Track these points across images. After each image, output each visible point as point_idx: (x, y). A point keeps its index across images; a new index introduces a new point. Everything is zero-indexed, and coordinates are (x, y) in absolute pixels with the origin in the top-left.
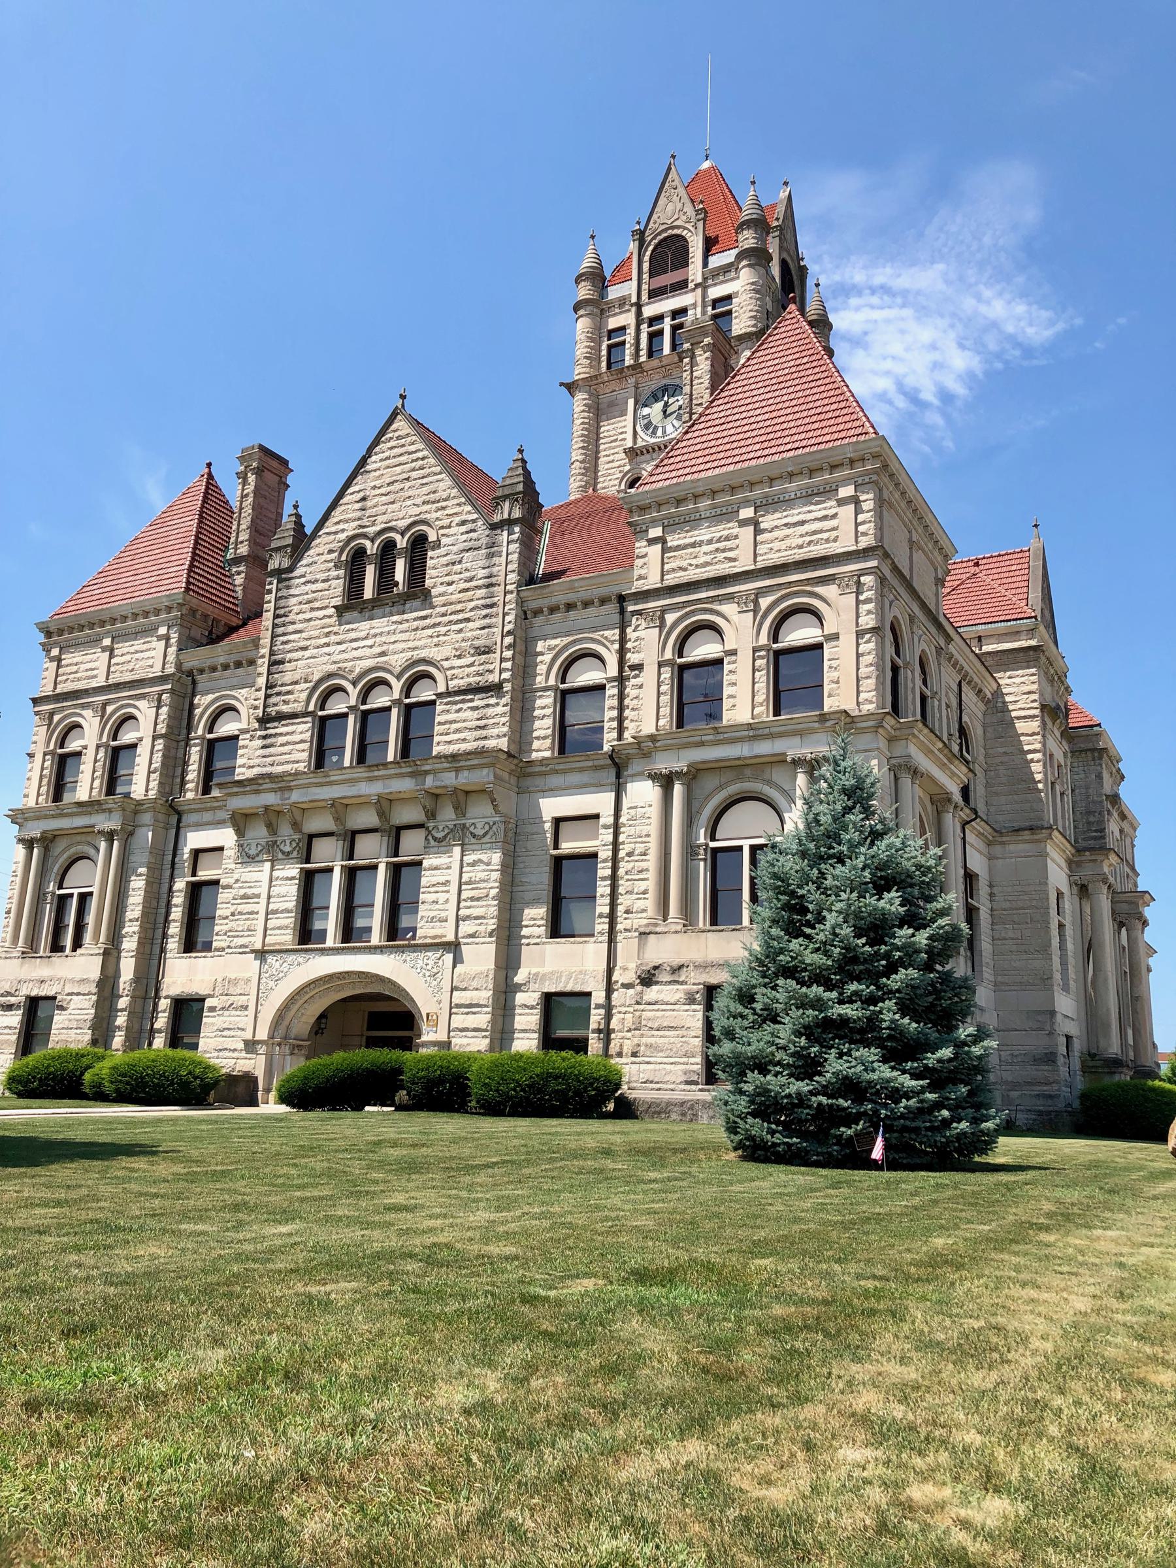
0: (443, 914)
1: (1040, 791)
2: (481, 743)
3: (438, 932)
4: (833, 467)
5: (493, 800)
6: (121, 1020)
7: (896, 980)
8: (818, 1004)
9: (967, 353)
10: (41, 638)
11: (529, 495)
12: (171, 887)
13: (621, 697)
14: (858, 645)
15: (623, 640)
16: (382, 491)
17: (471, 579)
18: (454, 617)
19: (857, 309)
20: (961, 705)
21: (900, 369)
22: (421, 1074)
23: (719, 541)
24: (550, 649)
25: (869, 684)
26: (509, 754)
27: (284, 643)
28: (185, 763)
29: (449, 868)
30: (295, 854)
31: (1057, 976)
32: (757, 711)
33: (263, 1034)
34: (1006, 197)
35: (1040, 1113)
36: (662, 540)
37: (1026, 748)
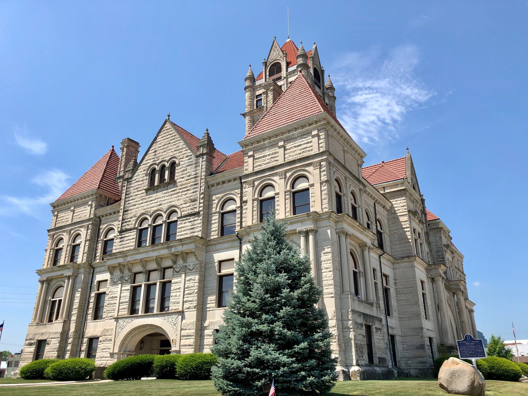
0: (178, 300)
1: (410, 242)
2: (192, 234)
3: (177, 307)
4: (310, 125)
5: (195, 255)
6: (69, 347)
7: (281, 313)
8: (249, 325)
9: (400, 106)
10: (52, 208)
11: (210, 144)
12: (90, 296)
13: (241, 213)
14: (321, 187)
15: (241, 193)
16: (162, 148)
17: (190, 176)
18: (184, 190)
19: (361, 95)
20: (375, 211)
21: (378, 113)
22: (159, 364)
23: (272, 154)
24: (217, 198)
25: (326, 201)
26: (201, 238)
27: (128, 204)
28: (96, 250)
29: (180, 282)
30: (129, 281)
31: (423, 314)
32: (287, 214)
33: (116, 351)
34: (406, 56)
35: (420, 369)
36: (253, 156)
37: (404, 227)
